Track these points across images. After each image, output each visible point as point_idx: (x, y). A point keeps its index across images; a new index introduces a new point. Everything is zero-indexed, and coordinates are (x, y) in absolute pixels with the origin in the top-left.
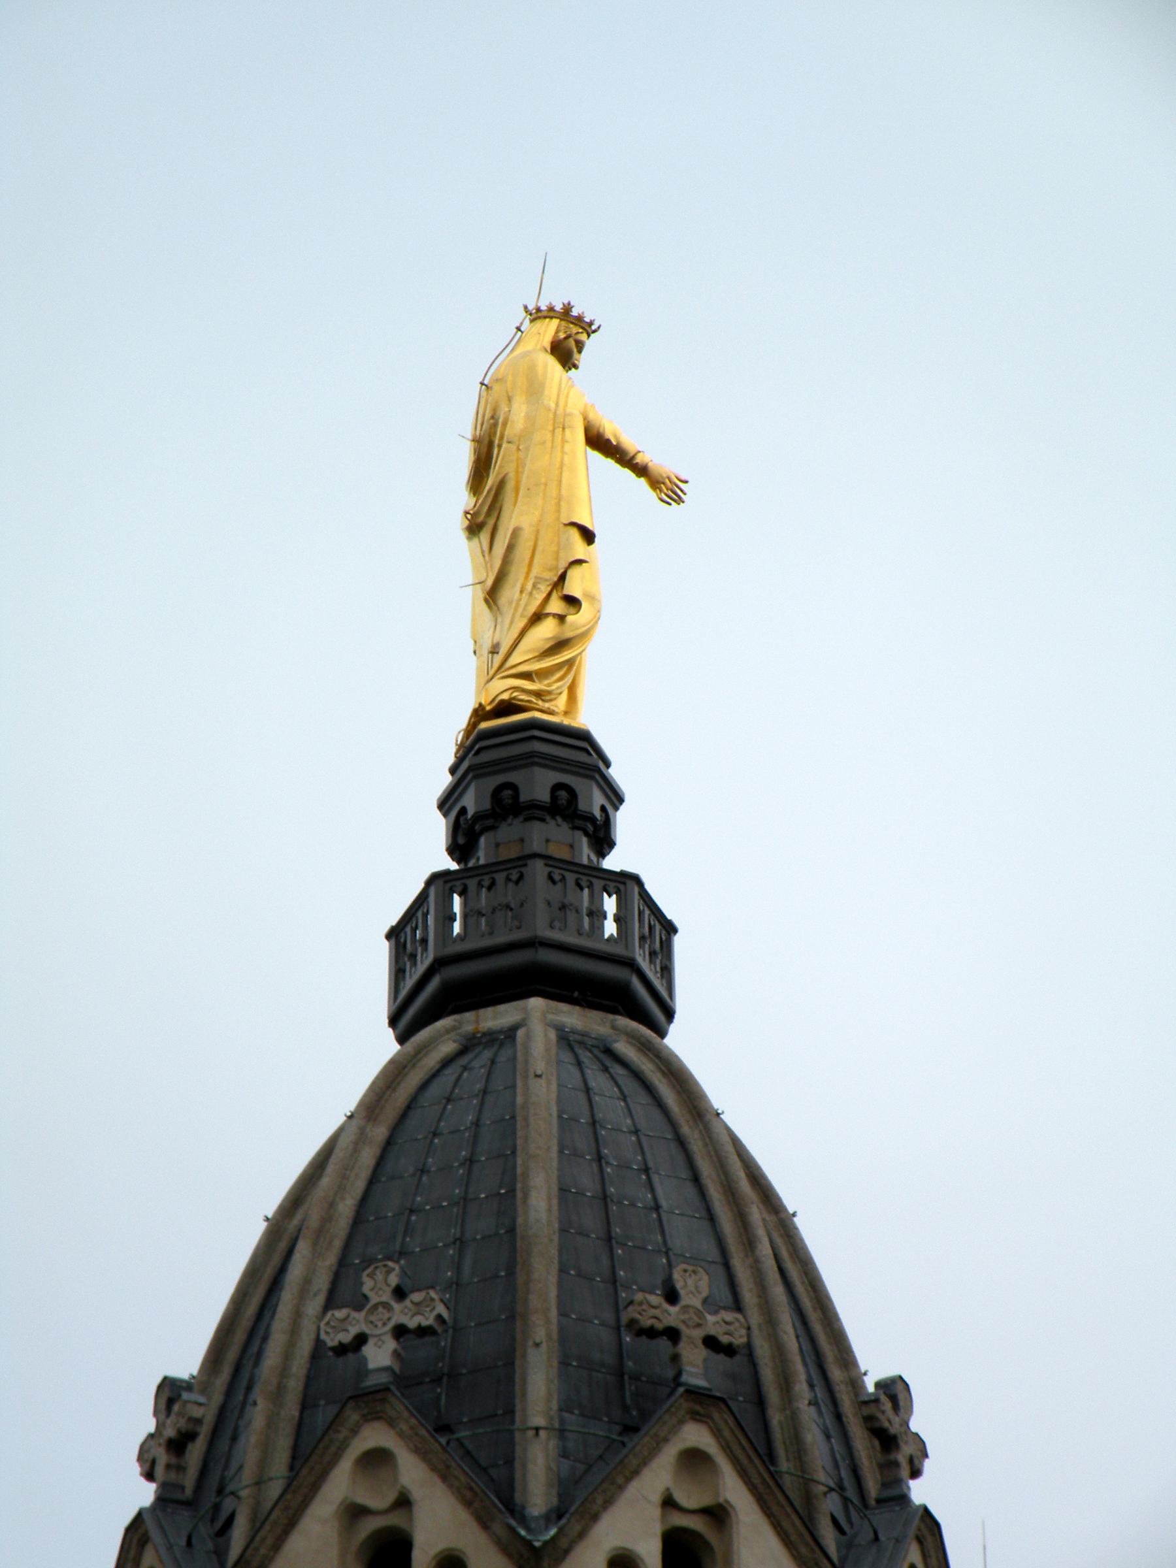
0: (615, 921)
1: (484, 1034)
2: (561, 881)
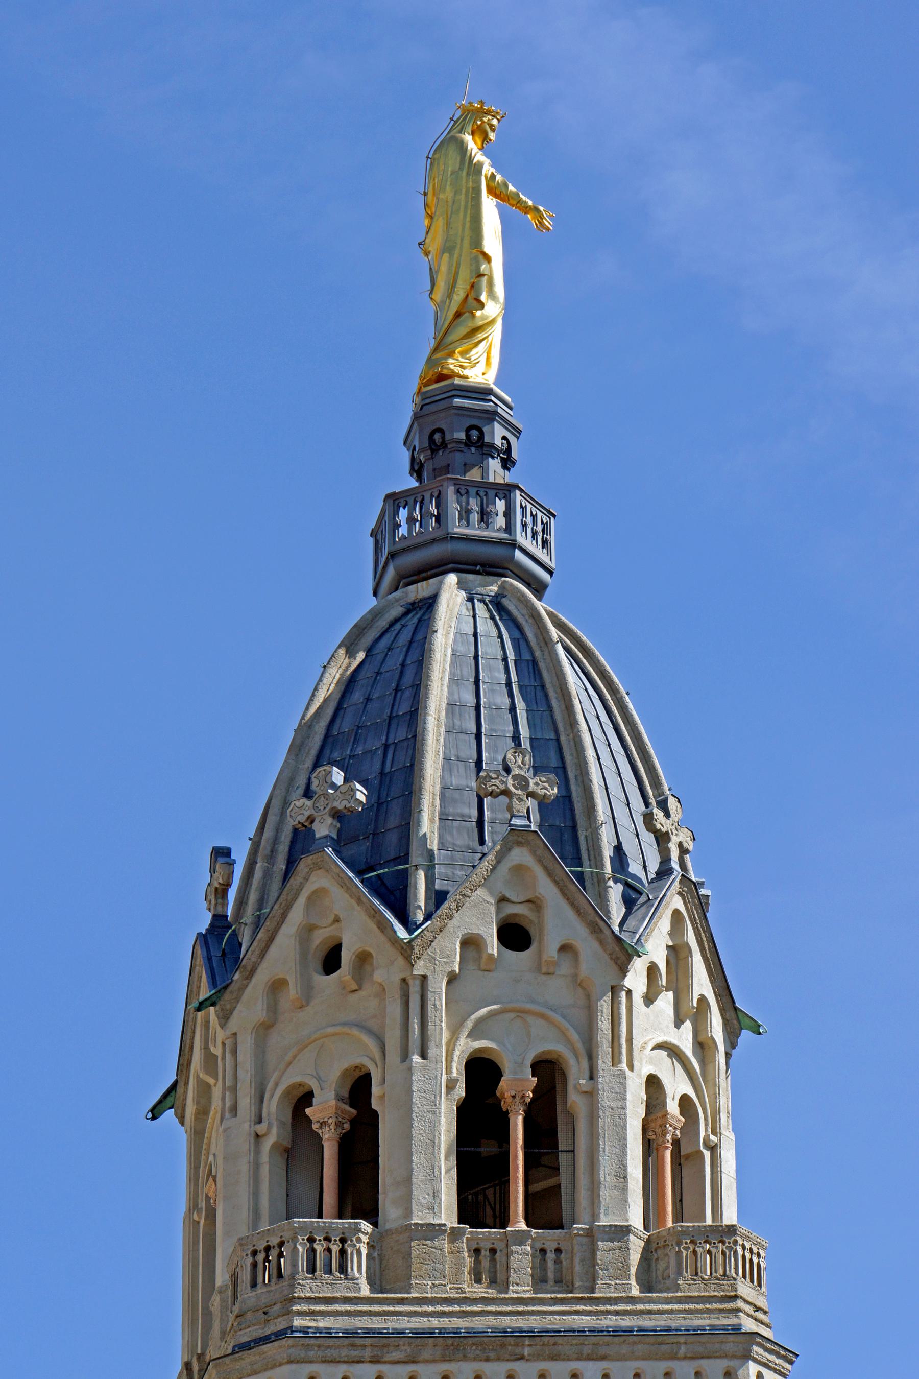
0: (504, 516)
1: (421, 600)
2: (466, 493)
